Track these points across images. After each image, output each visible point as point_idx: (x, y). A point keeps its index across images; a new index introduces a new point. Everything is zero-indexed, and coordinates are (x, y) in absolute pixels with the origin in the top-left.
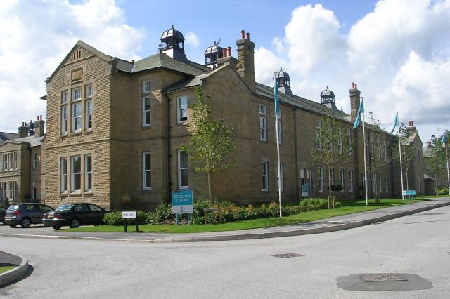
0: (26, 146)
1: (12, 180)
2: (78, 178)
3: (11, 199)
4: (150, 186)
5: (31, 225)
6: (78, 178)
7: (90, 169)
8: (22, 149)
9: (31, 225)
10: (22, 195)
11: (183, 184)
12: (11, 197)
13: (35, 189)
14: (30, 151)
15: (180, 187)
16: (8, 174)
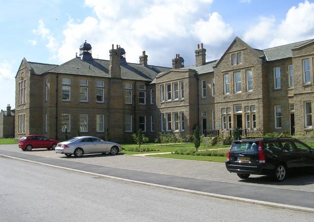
0: (193, 73)
1: (178, 110)
2: (169, 94)
3: (177, 131)
4: (311, 125)
5: (33, 149)
6: (169, 94)
7: (182, 88)
8: (190, 77)
9: (33, 149)
10: (190, 126)
11: (204, 96)
12: (177, 128)
13: (205, 121)
14: (198, 79)
15: (203, 97)
16: (172, 105)
